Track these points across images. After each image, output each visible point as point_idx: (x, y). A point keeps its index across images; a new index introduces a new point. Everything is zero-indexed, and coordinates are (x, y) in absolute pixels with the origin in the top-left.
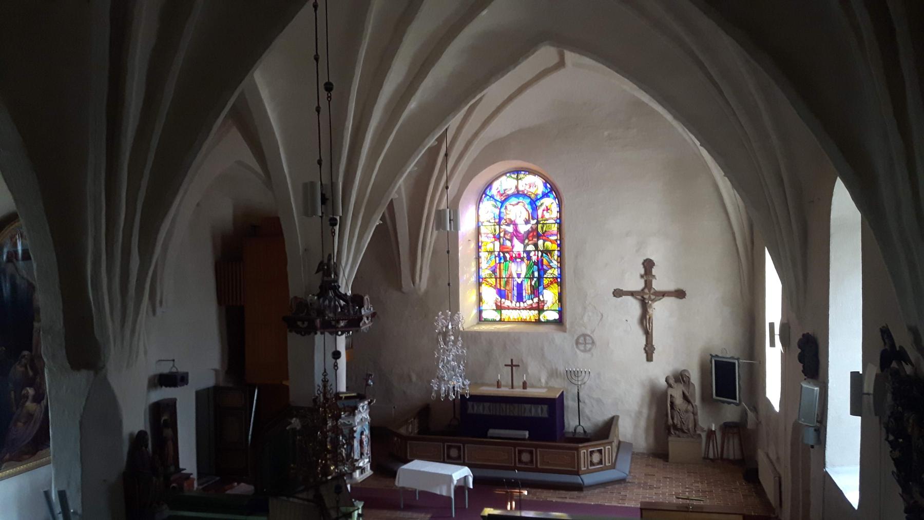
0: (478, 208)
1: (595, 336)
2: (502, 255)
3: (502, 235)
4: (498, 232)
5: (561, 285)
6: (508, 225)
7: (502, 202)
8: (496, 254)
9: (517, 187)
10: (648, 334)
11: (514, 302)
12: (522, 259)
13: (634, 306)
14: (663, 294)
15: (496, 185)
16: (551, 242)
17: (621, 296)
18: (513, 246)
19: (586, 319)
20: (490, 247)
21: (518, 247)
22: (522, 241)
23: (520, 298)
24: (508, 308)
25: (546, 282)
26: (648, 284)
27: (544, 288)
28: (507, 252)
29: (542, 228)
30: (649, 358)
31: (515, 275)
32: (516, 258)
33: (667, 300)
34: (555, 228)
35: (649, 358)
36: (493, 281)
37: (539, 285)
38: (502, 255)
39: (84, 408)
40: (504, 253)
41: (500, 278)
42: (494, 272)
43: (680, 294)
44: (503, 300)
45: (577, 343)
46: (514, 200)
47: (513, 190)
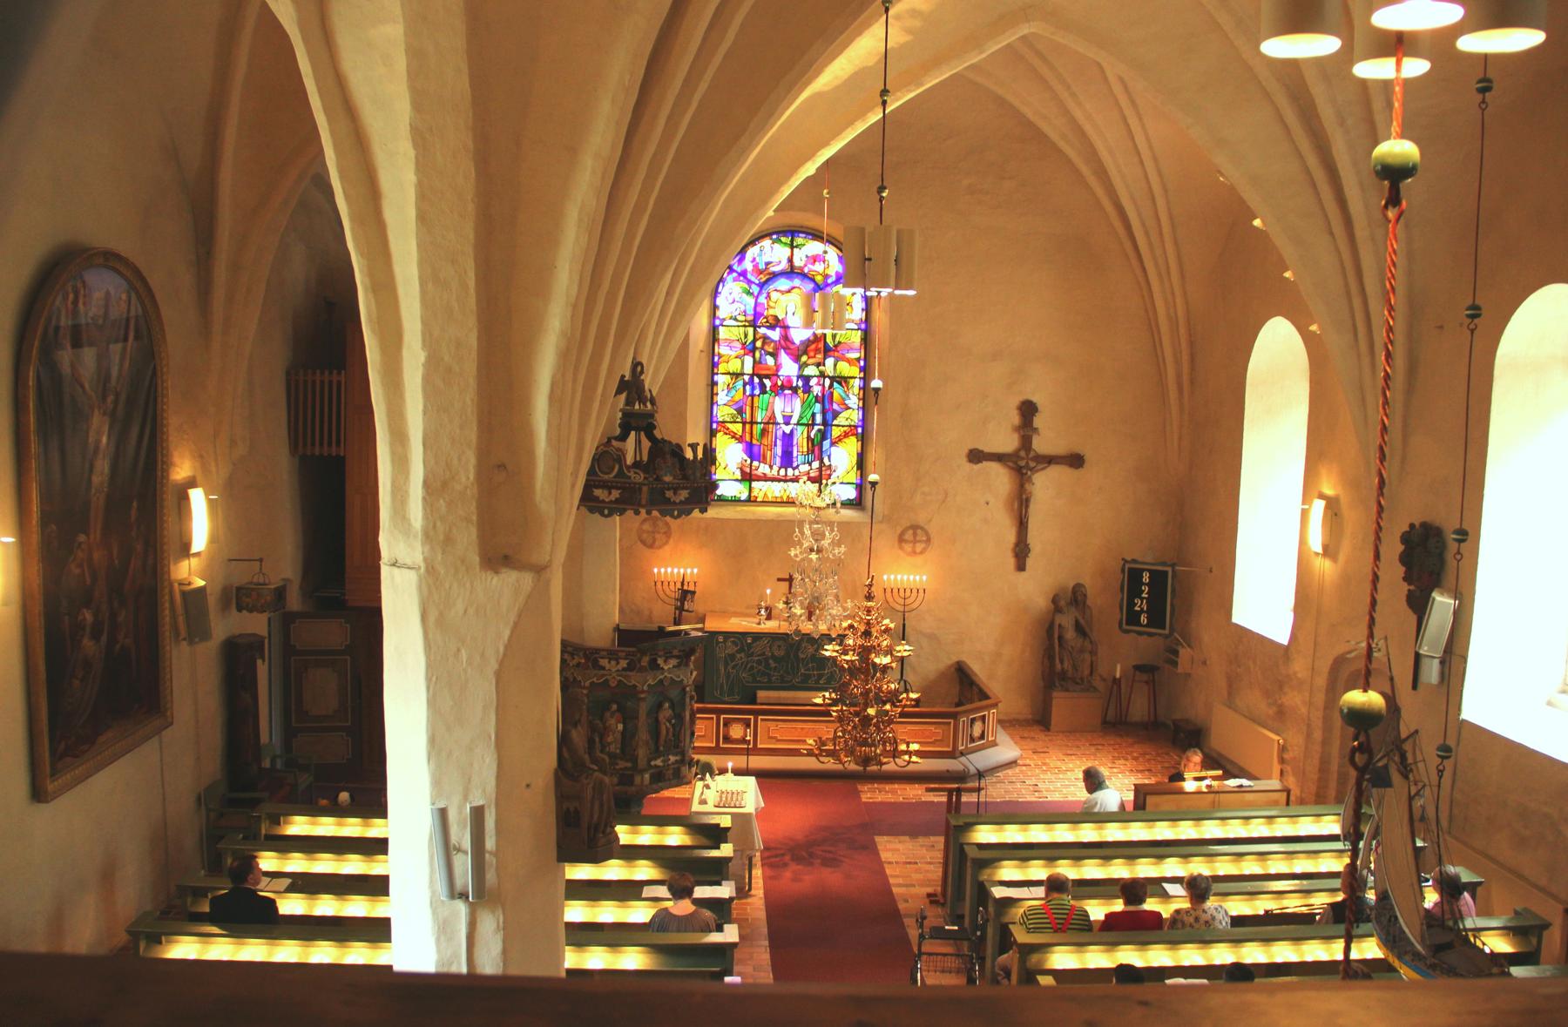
0: (716, 293)
1: (933, 529)
2: (756, 380)
3: (759, 344)
4: (750, 338)
5: (864, 439)
6: (772, 327)
7: (761, 286)
8: (747, 378)
9: (790, 260)
10: (1022, 525)
11: (775, 468)
12: (795, 390)
13: (1000, 478)
14: (1050, 460)
15: (752, 252)
16: (849, 361)
17: (979, 461)
18: (778, 367)
19: (918, 499)
20: (735, 366)
21: (789, 368)
22: (796, 359)
23: (787, 460)
24: (765, 478)
25: (836, 432)
26: (1026, 443)
27: (833, 444)
28: (767, 377)
29: (834, 336)
30: (1021, 567)
31: (780, 419)
32: (783, 387)
33: (1055, 471)
34: (856, 338)
35: (1021, 567)
36: (737, 428)
37: (824, 438)
38: (756, 380)
39: (506, 647)
40: (761, 377)
41: (752, 423)
42: (740, 411)
43: (1075, 461)
44: (755, 463)
45: (901, 540)
46: (783, 284)
47: (784, 265)
